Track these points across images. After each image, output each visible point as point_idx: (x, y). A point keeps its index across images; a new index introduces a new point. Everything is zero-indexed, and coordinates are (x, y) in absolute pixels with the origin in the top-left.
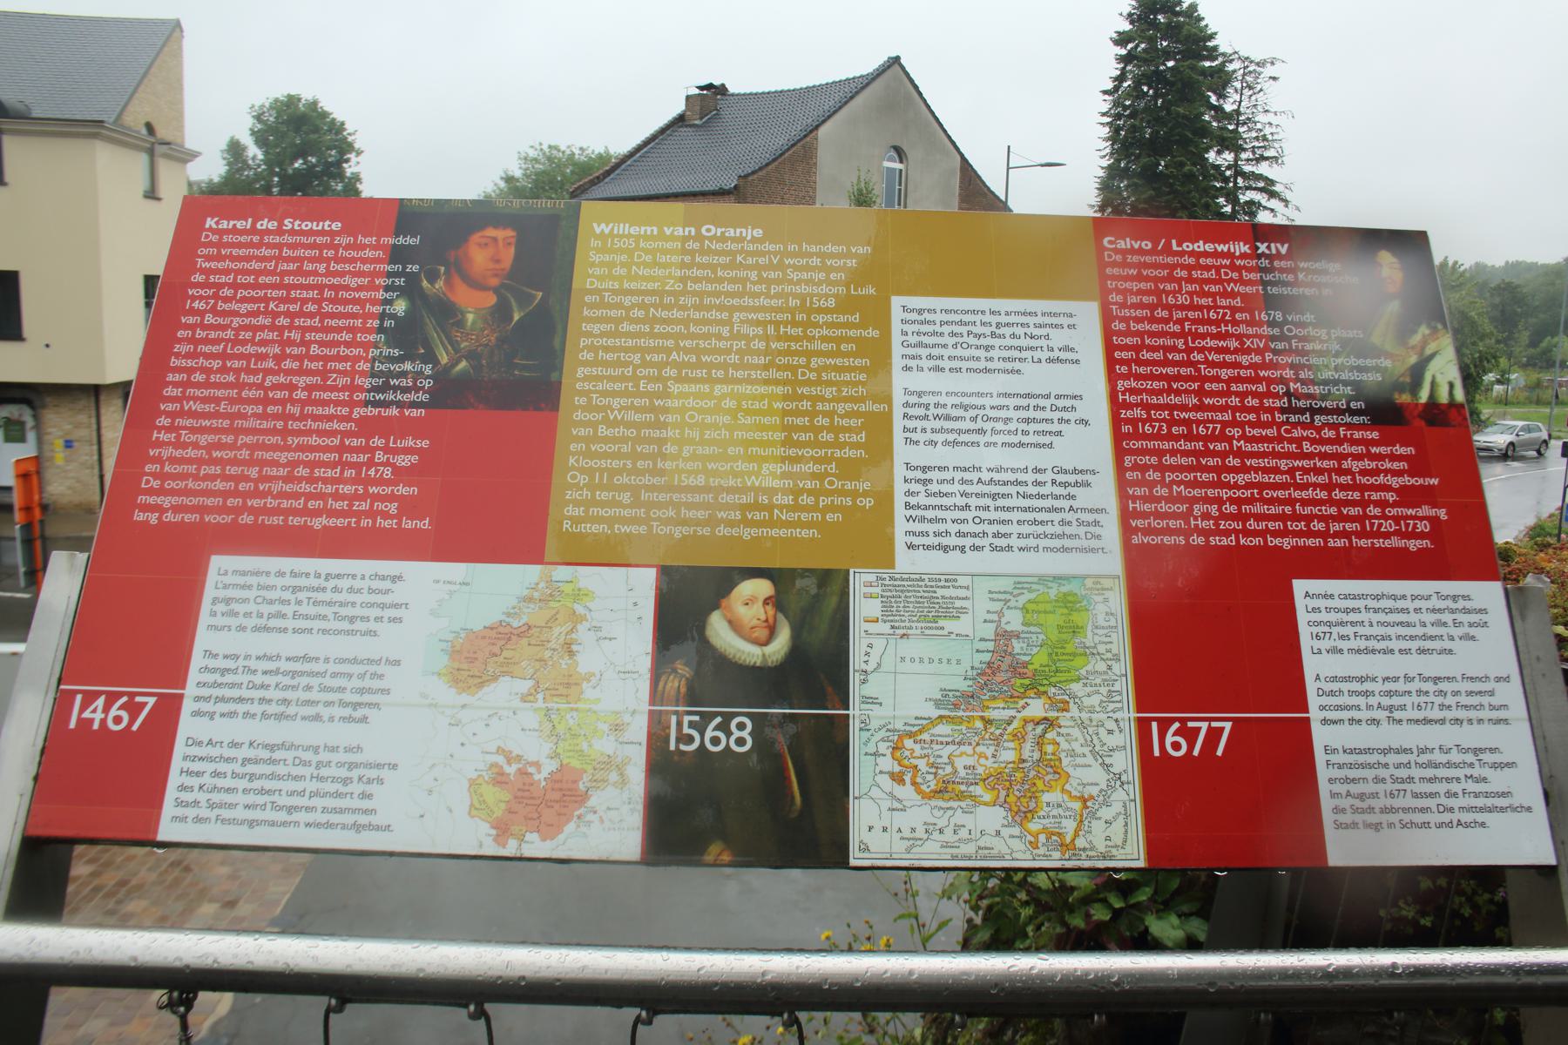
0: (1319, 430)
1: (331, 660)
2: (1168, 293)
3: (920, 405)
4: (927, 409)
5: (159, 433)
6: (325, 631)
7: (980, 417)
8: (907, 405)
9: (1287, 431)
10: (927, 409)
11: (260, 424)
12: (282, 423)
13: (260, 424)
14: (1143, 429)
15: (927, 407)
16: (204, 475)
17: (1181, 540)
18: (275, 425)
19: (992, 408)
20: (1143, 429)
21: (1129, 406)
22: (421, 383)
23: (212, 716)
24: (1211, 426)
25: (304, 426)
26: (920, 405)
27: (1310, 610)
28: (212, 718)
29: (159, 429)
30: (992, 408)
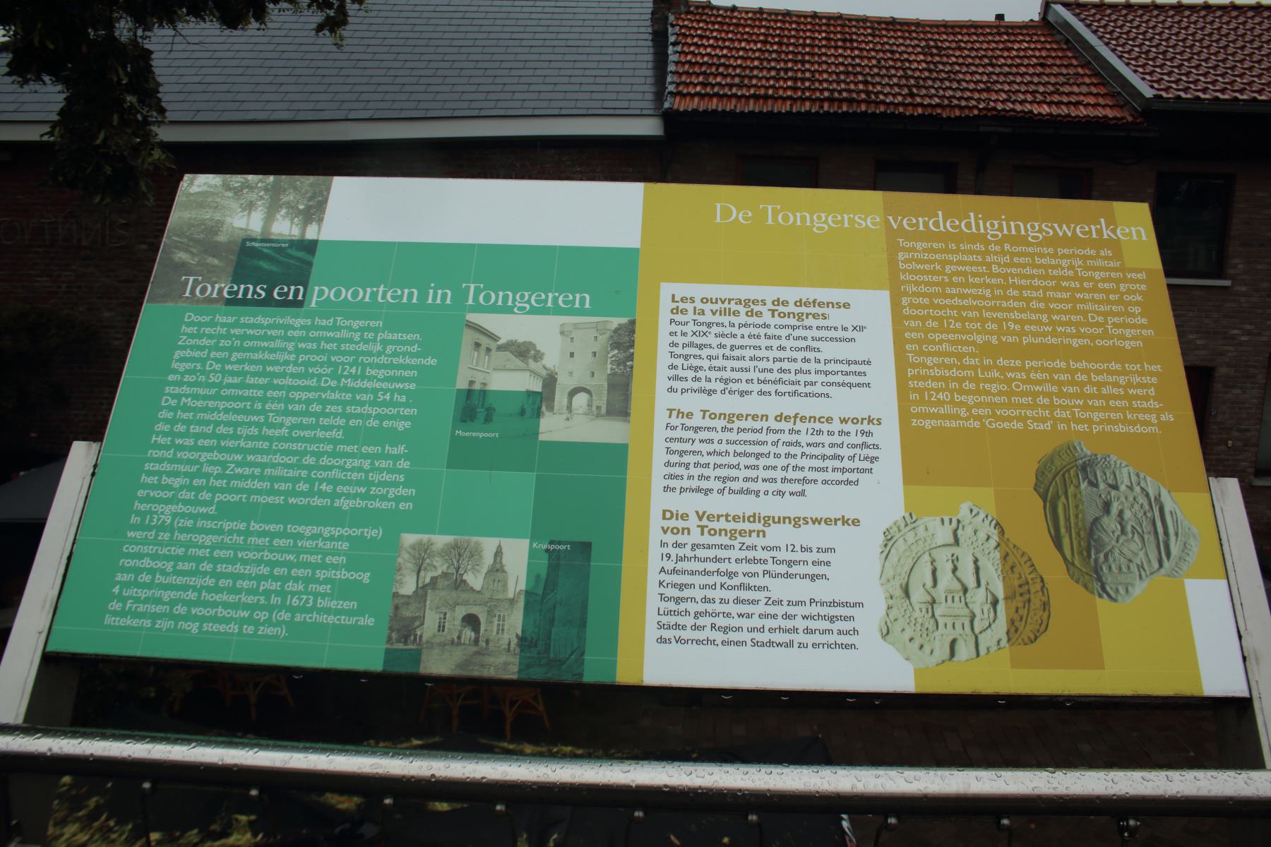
0: (1028, 372)
1: (770, 493)
2: (293, 594)
3: (680, 465)
4: (687, 468)
5: (157, 437)
6: (825, 482)
7: (857, 457)
8: (668, 464)
9: (1017, 386)
10: (687, 468)
11: (287, 473)
12: (306, 472)
13: (287, 473)
14: (291, 600)
15: (687, 466)
16: (263, 590)
17: (1020, 426)
18: (300, 473)
19: (809, 445)
20: (291, 600)
21: (909, 317)
22: (257, 615)
23: (757, 494)
24: (305, 597)
25: (215, 331)
26: (680, 465)
27: (862, 459)
28: (758, 496)
29: (158, 434)
30: (809, 445)
